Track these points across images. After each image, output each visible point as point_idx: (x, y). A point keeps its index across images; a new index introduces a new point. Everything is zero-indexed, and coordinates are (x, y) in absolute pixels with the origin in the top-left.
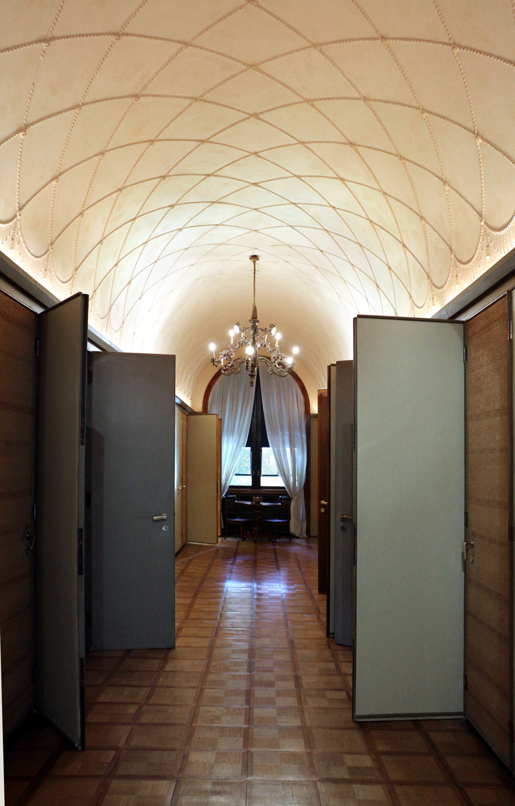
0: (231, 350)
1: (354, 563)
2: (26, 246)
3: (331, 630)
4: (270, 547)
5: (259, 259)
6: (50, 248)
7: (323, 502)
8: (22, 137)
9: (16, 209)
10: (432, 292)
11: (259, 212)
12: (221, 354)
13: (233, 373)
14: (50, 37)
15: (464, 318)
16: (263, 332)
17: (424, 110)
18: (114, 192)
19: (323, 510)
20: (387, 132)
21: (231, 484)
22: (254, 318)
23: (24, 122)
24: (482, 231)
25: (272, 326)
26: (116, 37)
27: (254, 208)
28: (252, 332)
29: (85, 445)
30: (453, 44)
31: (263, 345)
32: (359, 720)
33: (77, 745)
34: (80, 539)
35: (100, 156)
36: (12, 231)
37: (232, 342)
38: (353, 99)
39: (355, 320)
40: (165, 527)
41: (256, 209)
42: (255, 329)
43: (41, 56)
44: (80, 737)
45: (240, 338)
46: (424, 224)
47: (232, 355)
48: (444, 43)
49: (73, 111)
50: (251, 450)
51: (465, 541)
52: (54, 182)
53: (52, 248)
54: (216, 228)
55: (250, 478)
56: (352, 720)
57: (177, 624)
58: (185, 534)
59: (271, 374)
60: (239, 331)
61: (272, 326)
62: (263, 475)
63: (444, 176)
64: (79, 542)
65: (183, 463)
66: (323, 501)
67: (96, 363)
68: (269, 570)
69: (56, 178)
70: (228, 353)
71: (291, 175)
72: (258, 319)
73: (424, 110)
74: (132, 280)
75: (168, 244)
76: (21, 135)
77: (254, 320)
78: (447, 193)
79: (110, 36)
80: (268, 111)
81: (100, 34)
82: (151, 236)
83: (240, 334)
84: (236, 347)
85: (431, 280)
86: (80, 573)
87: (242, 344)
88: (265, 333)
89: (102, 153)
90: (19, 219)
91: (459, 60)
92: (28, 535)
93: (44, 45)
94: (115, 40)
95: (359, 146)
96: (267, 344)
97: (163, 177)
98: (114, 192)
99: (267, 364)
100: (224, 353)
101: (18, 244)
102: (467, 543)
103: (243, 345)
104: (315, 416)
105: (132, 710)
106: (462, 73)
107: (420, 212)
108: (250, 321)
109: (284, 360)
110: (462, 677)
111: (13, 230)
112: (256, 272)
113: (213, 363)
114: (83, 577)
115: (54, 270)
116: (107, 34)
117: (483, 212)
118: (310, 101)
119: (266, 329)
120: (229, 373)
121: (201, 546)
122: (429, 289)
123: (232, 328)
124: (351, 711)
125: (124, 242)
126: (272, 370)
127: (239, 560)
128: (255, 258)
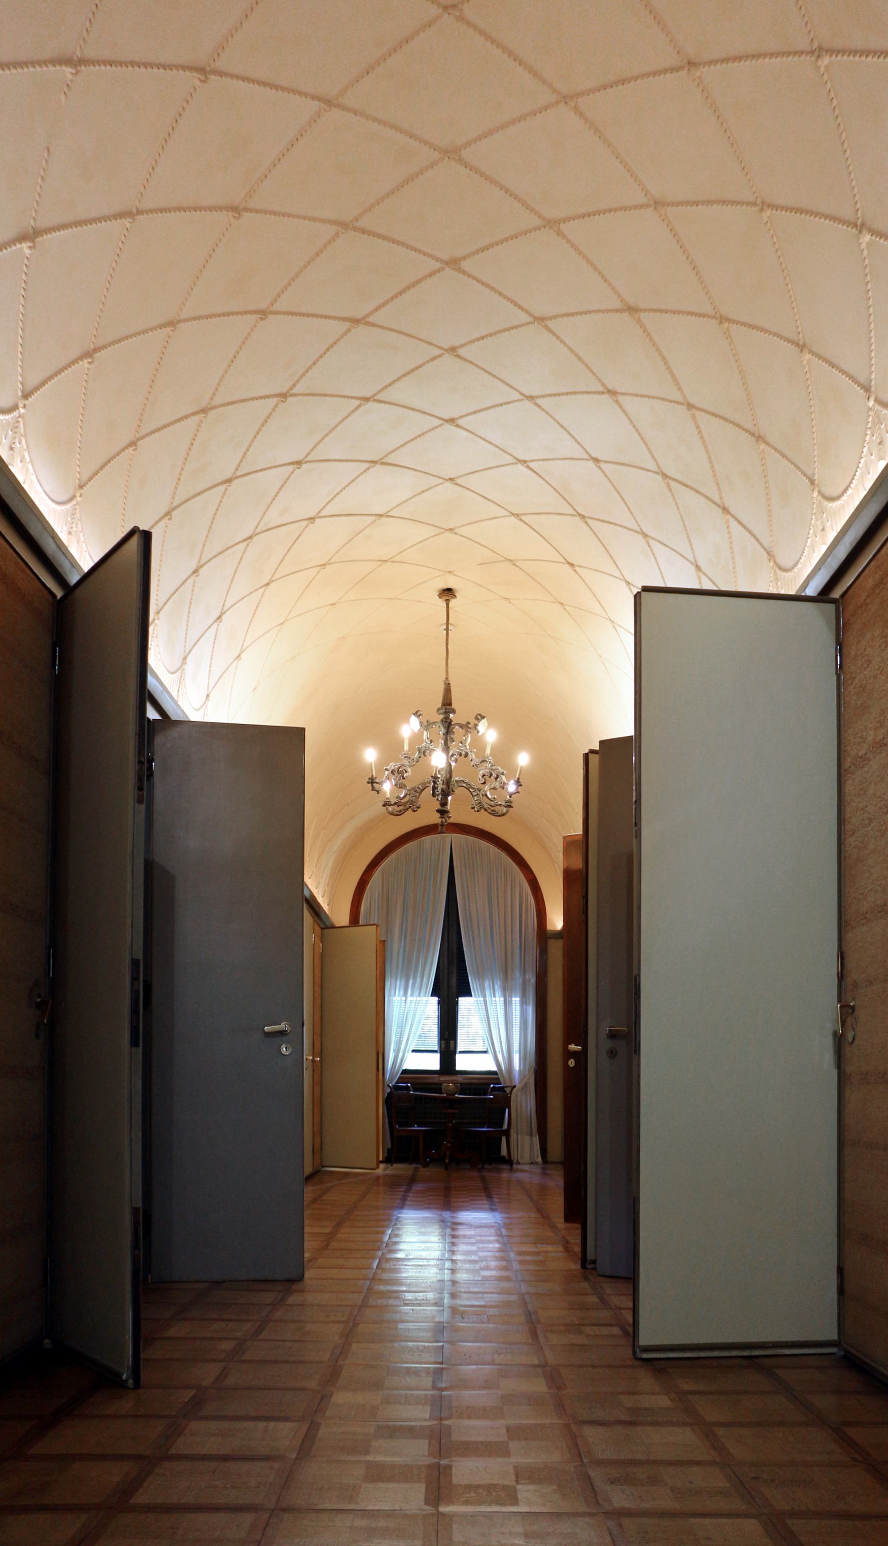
0: (406, 762)
1: (635, 1051)
2: (34, 471)
3: (590, 1255)
4: (475, 1173)
5: (455, 596)
6: (78, 494)
7: (572, 1047)
8: (27, 252)
9: (17, 394)
10: (777, 584)
11: (457, 487)
12: (387, 770)
13: (407, 809)
14: (79, 56)
15: (836, 594)
16: (463, 729)
17: (764, 205)
18: (193, 414)
19: (572, 1063)
20: (695, 270)
21: (404, 1068)
22: (447, 705)
23: (32, 223)
24: (870, 419)
25: (480, 717)
26: (200, 76)
27: (447, 478)
28: (443, 731)
29: (145, 804)
30: (817, 50)
31: (463, 753)
32: (645, 1356)
33: (126, 1377)
34: (134, 979)
35: (167, 329)
36: (10, 432)
37: (406, 748)
38: (635, 207)
39: (637, 597)
40: (286, 1048)
41: (451, 479)
42: (448, 725)
43: (63, 94)
44: (130, 1362)
45: (422, 741)
46: (763, 451)
47: (406, 772)
48: (801, 53)
49: (119, 221)
50: (439, 1002)
51: (839, 1001)
52: (85, 361)
53: (81, 494)
54: (378, 521)
55: (437, 1056)
56: (632, 1357)
57: (307, 1255)
58: (318, 1150)
59: (478, 811)
60: (419, 727)
61: (479, 717)
62: (460, 1052)
63: (801, 335)
64: (132, 985)
65: (315, 961)
66: (573, 1045)
67: (159, 740)
68: (473, 1198)
69: (88, 355)
70: (399, 768)
71: (518, 396)
72: (454, 706)
73: (764, 205)
74: (224, 613)
75: (291, 547)
76: (25, 246)
77: (446, 709)
78: (806, 369)
79: (188, 73)
80: (477, 252)
81: (170, 67)
82: (258, 524)
83: (420, 734)
84: (413, 757)
85: (775, 562)
86: (134, 1043)
87: (424, 753)
88: (467, 732)
89: (172, 324)
90: (23, 413)
91: (828, 82)
92: (39, 1000)
93: (67, 71)
94: (197, 83)
95: (645, 310)
96: (471, 752)
97: (283, 396)
98: (193, 414)
99: (470, 792)
100: (392, 768)
101: (21, 462)
102: (843, 1004)
103: (424, 753)
104: (558, 935)
105: (227, 1346)
106: (833, 107)
107: (756, 428)
108: (438, 710)
109: (501, 778)
110: (835, 1269)
111: (11, 431)
112: (450, 628)
113: (372, 785)
114: (140, 1050)
115: (85, 540)
116: (184, 68)
117: (872, 380)
118: (552, 224)
119: (469, 723)
120: (401, 811)
121: (347, 1174)
122: (771, 581)
123: (407, 720)
124: (631, 1298)
125: (211, 527)
126: (479, 803)
127: (418, 1187)
128: (448, 593)
